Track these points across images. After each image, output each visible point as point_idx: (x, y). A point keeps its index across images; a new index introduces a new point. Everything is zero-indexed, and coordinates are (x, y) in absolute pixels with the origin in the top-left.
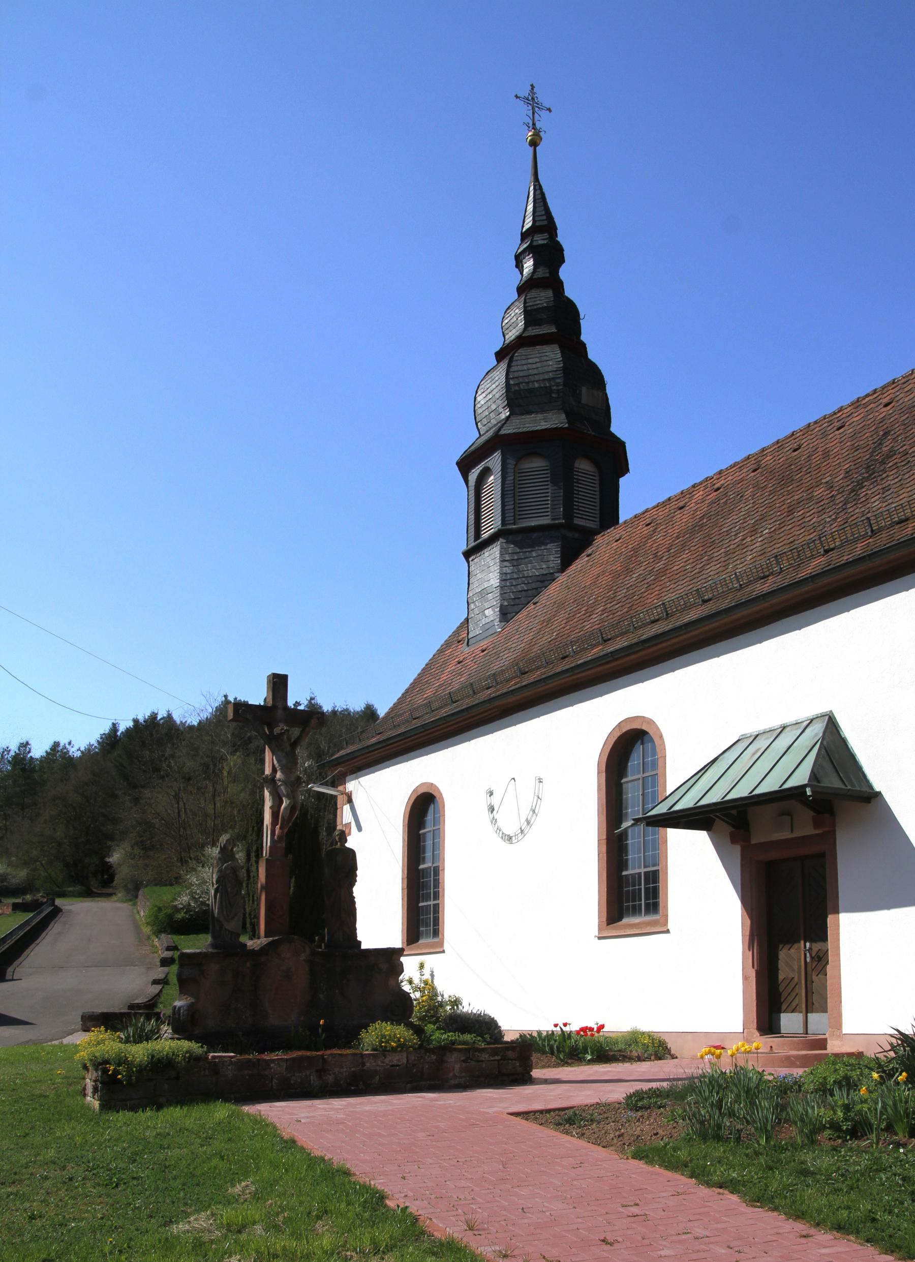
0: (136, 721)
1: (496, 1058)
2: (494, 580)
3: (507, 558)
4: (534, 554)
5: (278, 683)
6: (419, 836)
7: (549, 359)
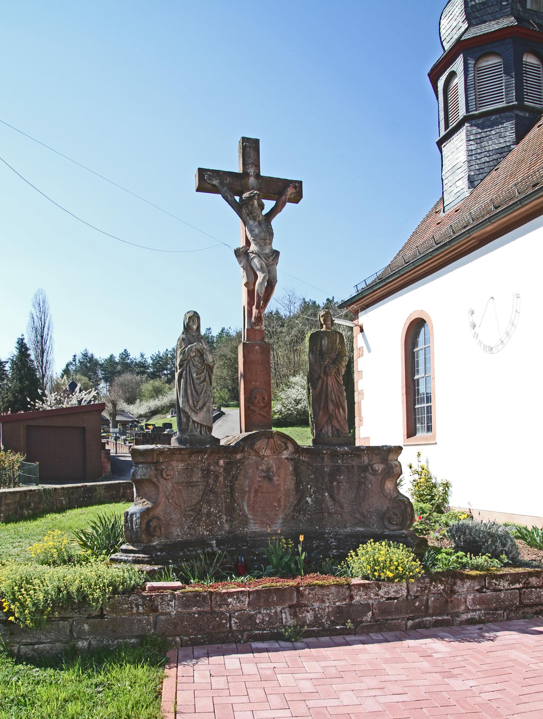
1: (517, 586)
2: (462, 156)
3: (472, 137)
4: (493, 132)
5: (250, 148)
6: (413, 353)
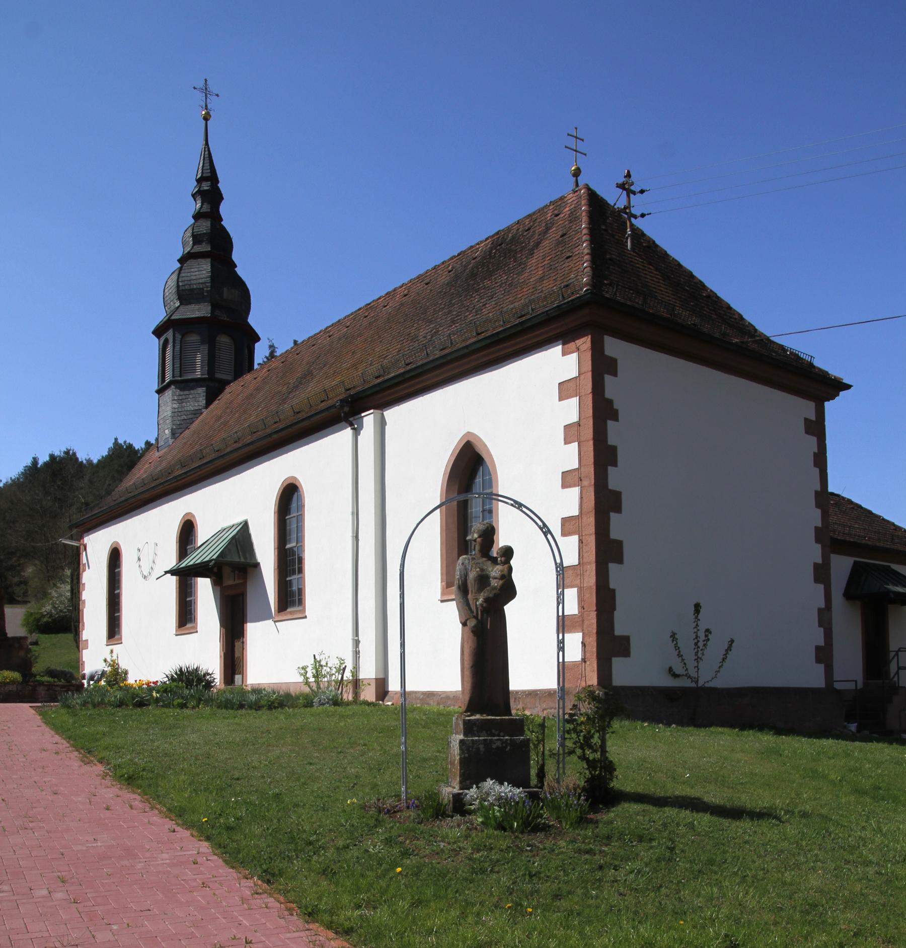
0: (52, 457)
7: (202, 271)
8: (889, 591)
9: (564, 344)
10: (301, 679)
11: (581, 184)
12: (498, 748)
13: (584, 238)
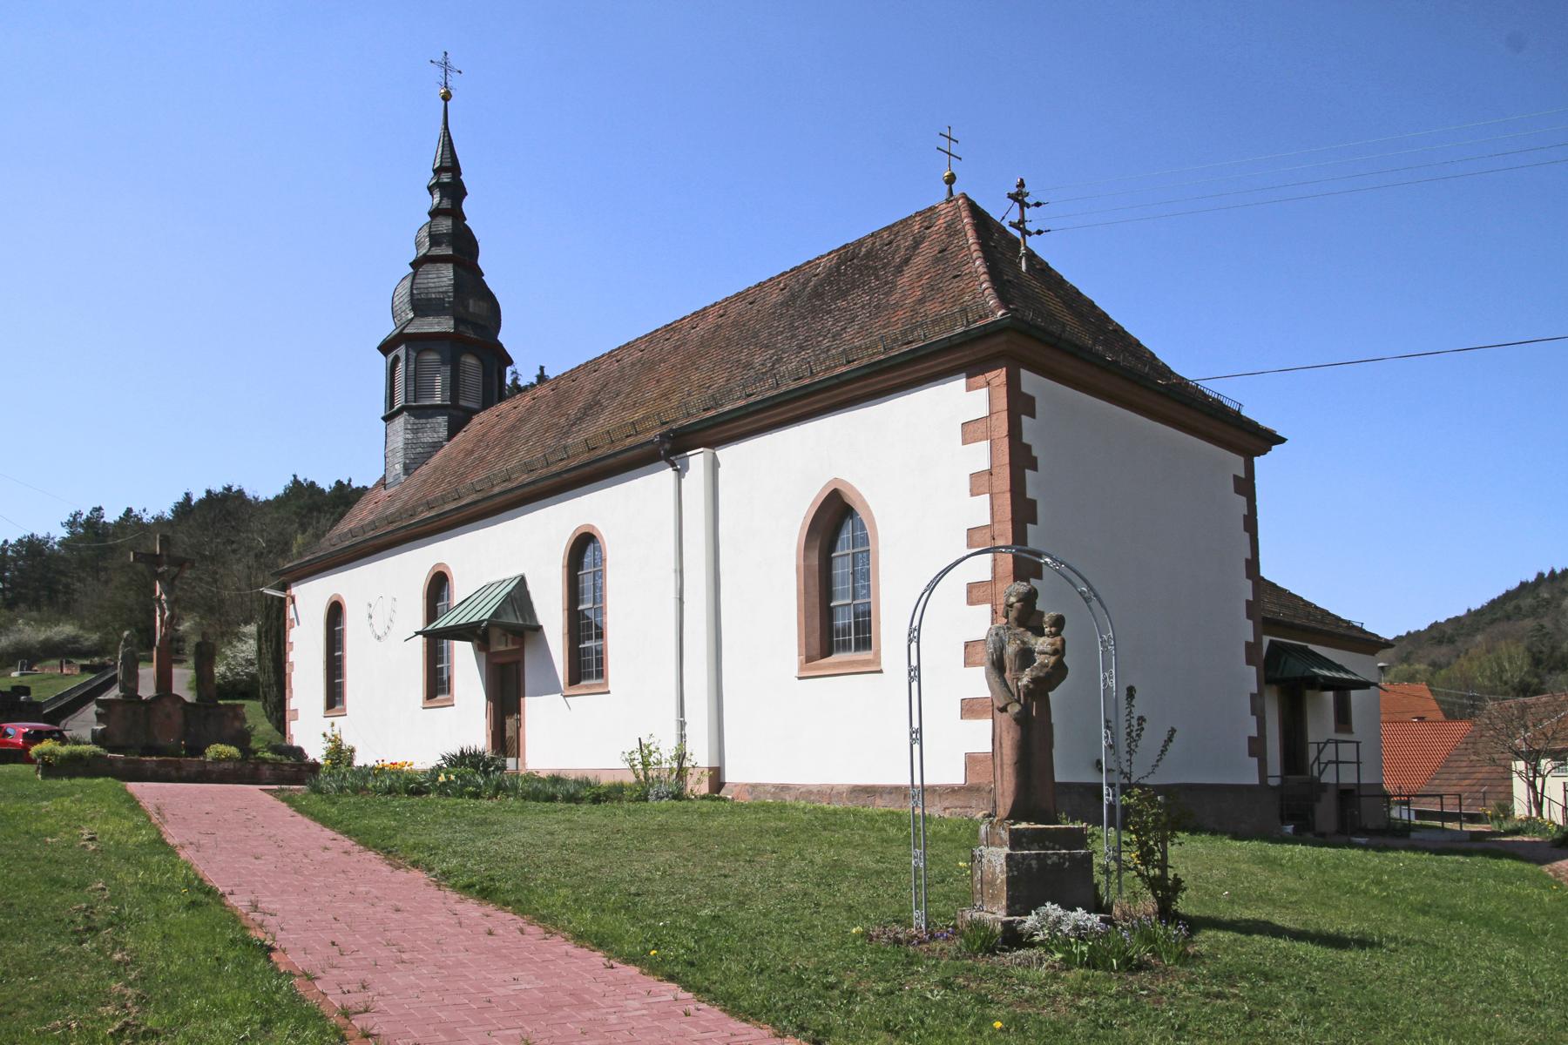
7: (443, 278)
8: (1317, 676)
9: (968, 377)
10: (627, 765)
11: (956, 193)
12: (1054, 864)
13: (975, 255)
